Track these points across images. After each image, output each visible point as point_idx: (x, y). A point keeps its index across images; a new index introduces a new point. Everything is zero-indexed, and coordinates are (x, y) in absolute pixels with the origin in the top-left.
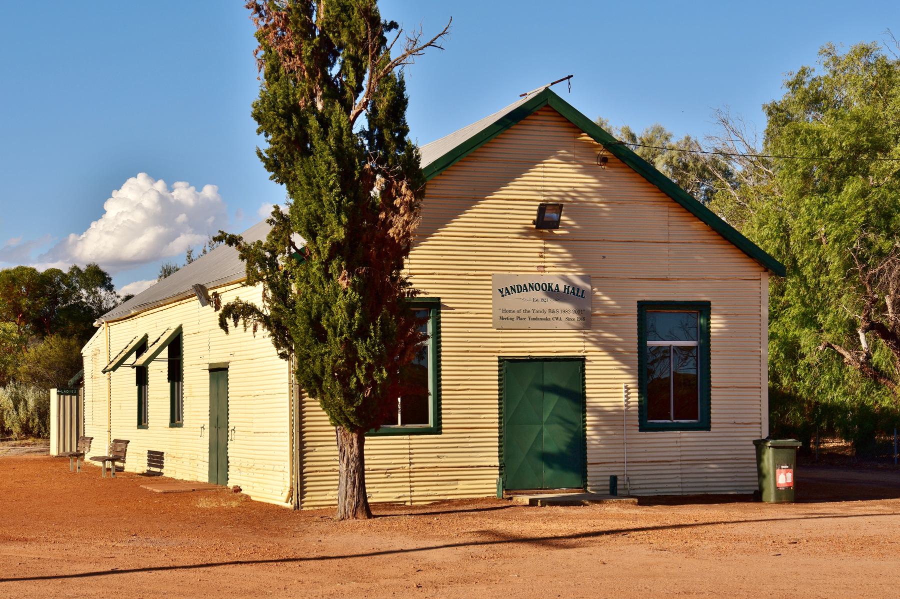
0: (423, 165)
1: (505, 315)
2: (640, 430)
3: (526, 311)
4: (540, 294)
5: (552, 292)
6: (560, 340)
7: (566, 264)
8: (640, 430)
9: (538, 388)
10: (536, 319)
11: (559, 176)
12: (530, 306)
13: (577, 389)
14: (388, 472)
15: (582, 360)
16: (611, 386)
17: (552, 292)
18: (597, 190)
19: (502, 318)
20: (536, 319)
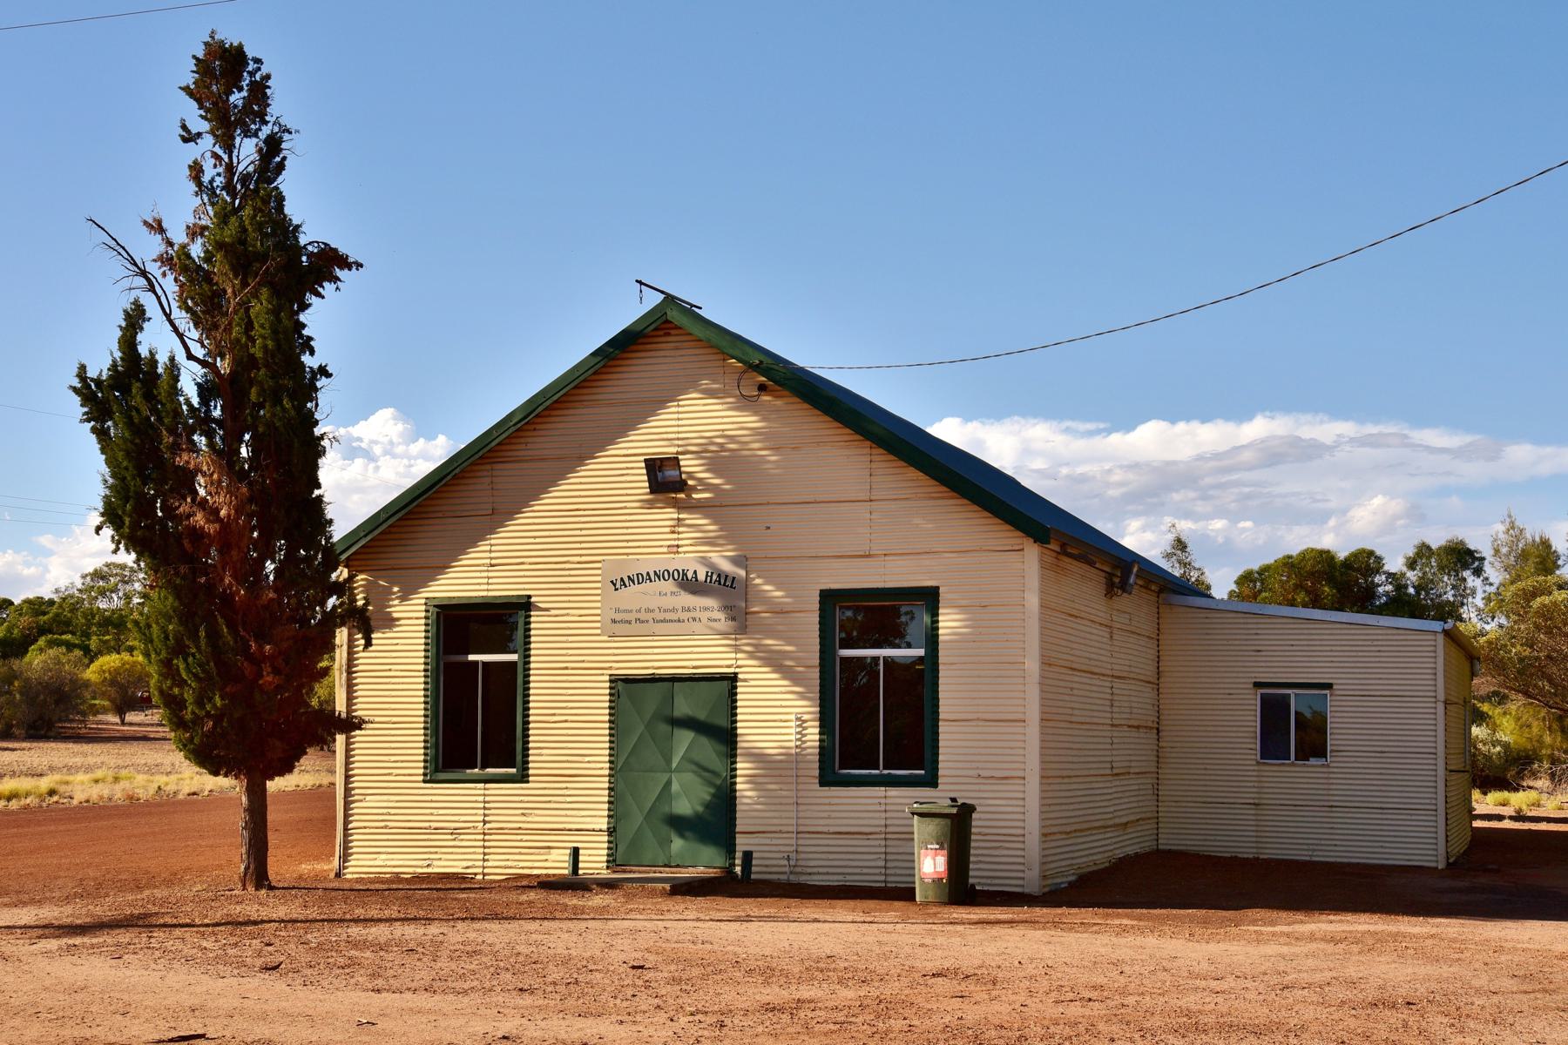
0: (339, 532)
1: (618, 617)
2: (822, 784)
5: (688, 584)
6: (700, 648)
9: (670, 717)
11: (697, 420)
12: (654, 603)
13: (723, 722)
14: (455, 832)
15: (733, 678)
16: (778, 716)
17: (688, 584)
19: (614, 621)
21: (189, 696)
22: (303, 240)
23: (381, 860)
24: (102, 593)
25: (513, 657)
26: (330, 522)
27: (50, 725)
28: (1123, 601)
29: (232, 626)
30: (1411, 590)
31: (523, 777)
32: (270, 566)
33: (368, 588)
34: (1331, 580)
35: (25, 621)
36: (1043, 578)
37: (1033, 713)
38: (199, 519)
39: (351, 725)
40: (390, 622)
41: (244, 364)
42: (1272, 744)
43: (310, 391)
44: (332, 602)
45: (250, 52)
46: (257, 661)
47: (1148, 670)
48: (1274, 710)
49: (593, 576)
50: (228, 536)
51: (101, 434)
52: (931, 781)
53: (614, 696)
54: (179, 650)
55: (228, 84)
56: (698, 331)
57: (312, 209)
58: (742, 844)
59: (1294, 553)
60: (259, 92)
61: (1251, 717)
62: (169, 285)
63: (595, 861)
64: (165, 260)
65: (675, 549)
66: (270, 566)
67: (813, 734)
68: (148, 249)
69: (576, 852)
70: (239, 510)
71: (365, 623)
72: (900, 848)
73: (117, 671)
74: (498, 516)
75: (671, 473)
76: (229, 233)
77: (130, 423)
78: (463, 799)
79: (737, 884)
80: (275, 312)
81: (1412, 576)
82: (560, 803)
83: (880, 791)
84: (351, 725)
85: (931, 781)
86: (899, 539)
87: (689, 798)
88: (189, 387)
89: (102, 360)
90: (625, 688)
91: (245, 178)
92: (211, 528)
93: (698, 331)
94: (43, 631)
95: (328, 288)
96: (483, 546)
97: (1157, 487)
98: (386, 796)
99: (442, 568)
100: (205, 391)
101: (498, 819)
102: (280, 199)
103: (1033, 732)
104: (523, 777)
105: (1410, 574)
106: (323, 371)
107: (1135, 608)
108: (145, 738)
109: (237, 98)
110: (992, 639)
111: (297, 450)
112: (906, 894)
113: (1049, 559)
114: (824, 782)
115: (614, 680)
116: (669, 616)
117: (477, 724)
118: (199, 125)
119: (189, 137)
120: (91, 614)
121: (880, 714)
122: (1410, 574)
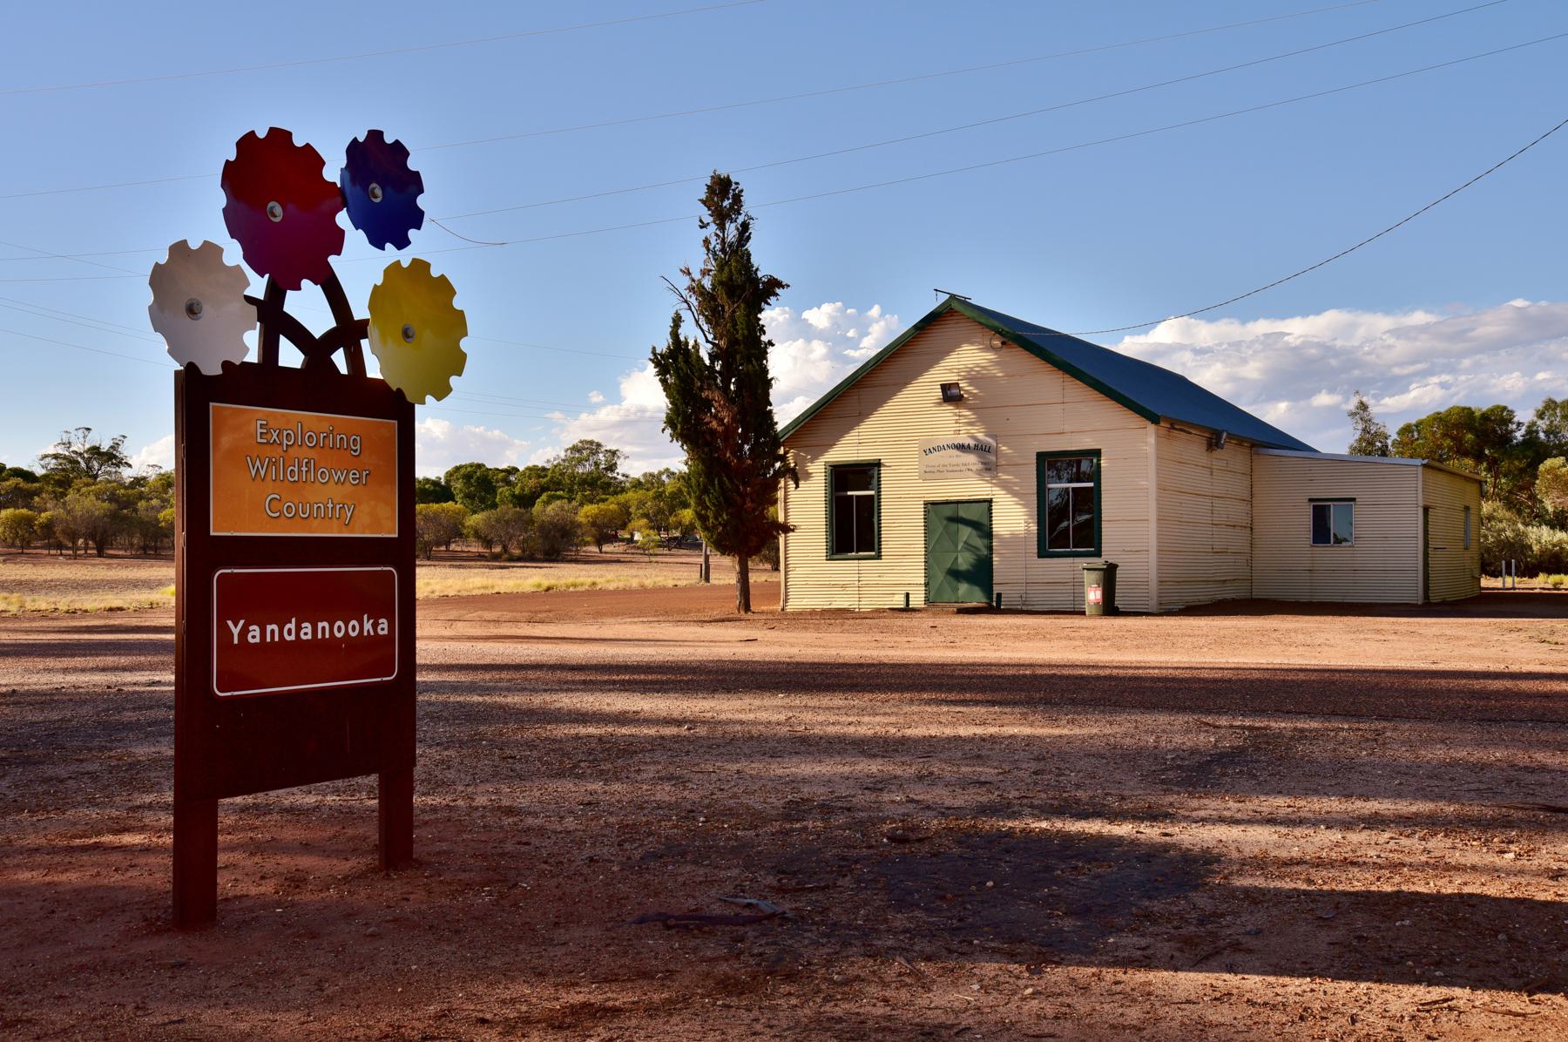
0: (779, 427)
4: (956, 452)
5: (962, 448)
6: (972, 487)
7: (970, 424)
9: (957, 523)
11: (968, 358)
12: (946, 461)
13: (985, 521)
14: (843, 586)
15: (990, 501)
16: (1013, 518)
17: (962, 448)
18: (997, 363)
21: (710, 514)
22: (760, 275)
23: (805, 602)
24: (580, 461)
27: (558, 552)
28: (1218, 453)
29: (731, 481)
30: (1542, 435)
31: (879, 557)
32: (747, 447)
33: (795, 457)
34: (1471, 429)
35: (532, 482)
36: (1158, 443)
38: (714, 424)
39: (786, 529)
40: (808, 476)
41: (733, 342)
43: (763, 354)
44: (778, 465)
45: (733, 179)
46: (743, 496)
47: (1245, 494)
49: (916, 449)
50: (729, 433)
51: (664, 381)
52: (1098, 554)
53: (926, 512)
54: (705, 491)
55: (722, 197)
56: (968, 313)
57: (764, 261)
58: (996, 589)
59: (1442, 410)
60: (737, 199)
61: (1307, 519)
62: (693, 301)
63: (918, 600)
64: (691, 289)
65: (958, 432)
66: (747, 447)
67: (1034, 528)
68: (683, 283)
69: (907, 595)
70: (734, 419)
71: (796, 476)
72: (1078, 587)
73: (596, 516)
74: (861, 416)
75: (955, 391)
76: (724, 276)
77: (678, 377)
78: (847, 569)
79: (993, 607)
80: (748, 316)
81: (1543, 424)
82: (902, 564)
83: (1070, 560)
84: (786, 529)
85: (1098, 554)
87: (964, 561)
88: (704, 355)
89: (663, 344)
90: (931, 507)
91: (731, 245)
92: (720, 429)
93: (968, 313)
94: (544, 489)
95: (772, 300)
96: (854, 433)
97: (1302, 372)
98: (807, 564)
99: (831, 445)
100: (712, 357)
101: (865, 579)
102: (749, 255)
103: (1153, 526)
104: (879, 557)
105: (1540, 422)
106: (771, 343)
107: (1231, 457)
108: (618, 561)
109: (726, 203)
110: (1139, 473)
111: (759, 384)
112: (1083, 613)
113: (1163, 432)
114: (1040, 556)
115: (926, 504)
117: (854, 528)
118: (708, 219)
119: (703, 226)
120: (573, 477)
121: (1071, 520)
122: (1540, 422)
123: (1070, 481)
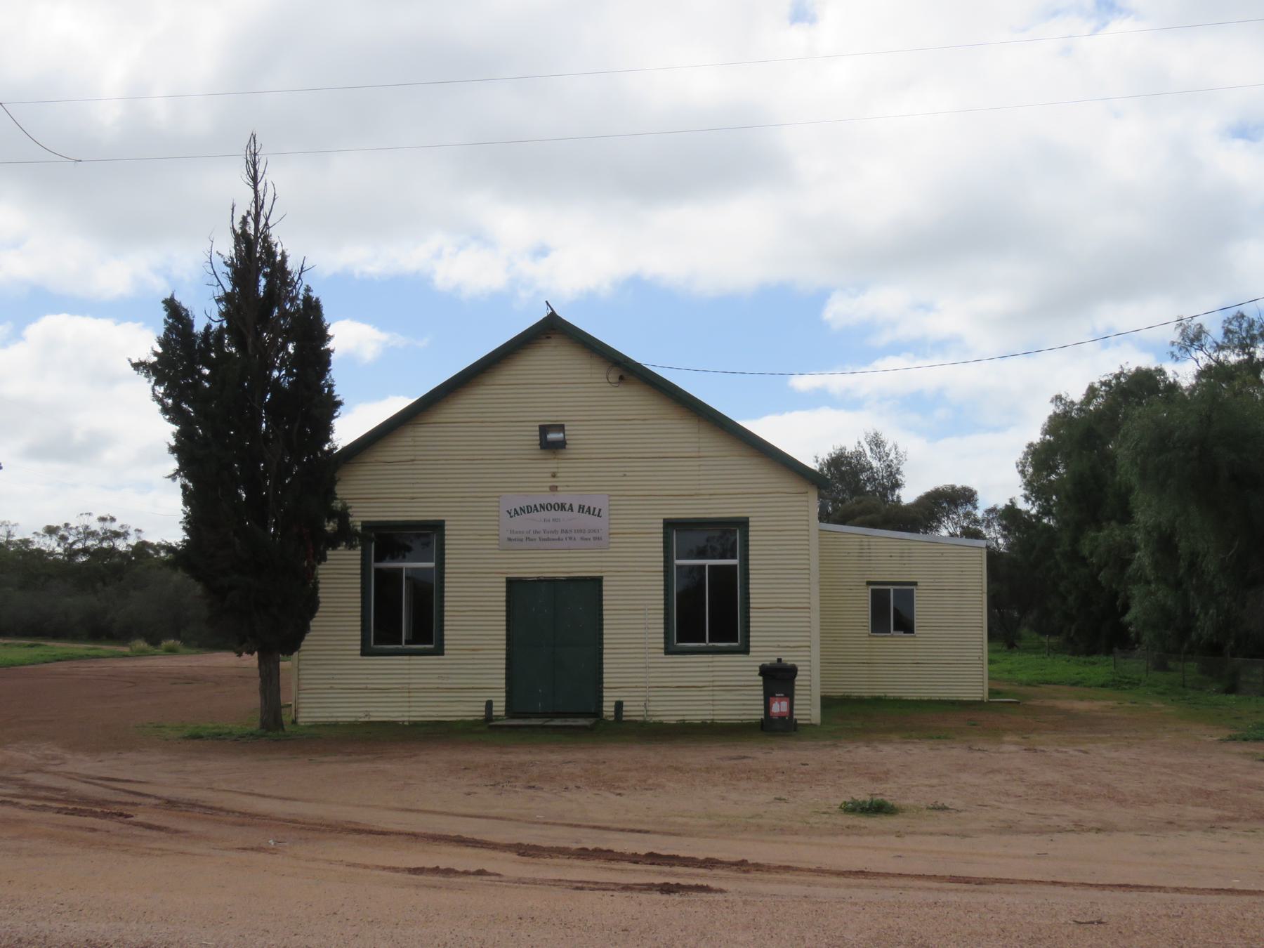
1: (513, 536)
2: (666, 653)
3: (536, 532)
8: (666, 653)
10: (548, 539)
19: (510, 539)
20: (548, 539)
25: (432, 565)
26: (173, 450)
31: (439, 651)
37: (815, 602)
42: (880, 622)
48: (879, 599)
85: (745, 650)
86: (717, 491)
98: (337, 673)
103: (815, 616)
104: (439, 651)
116: (551, 536)
117: (405, 616)
123: (701, 554)
